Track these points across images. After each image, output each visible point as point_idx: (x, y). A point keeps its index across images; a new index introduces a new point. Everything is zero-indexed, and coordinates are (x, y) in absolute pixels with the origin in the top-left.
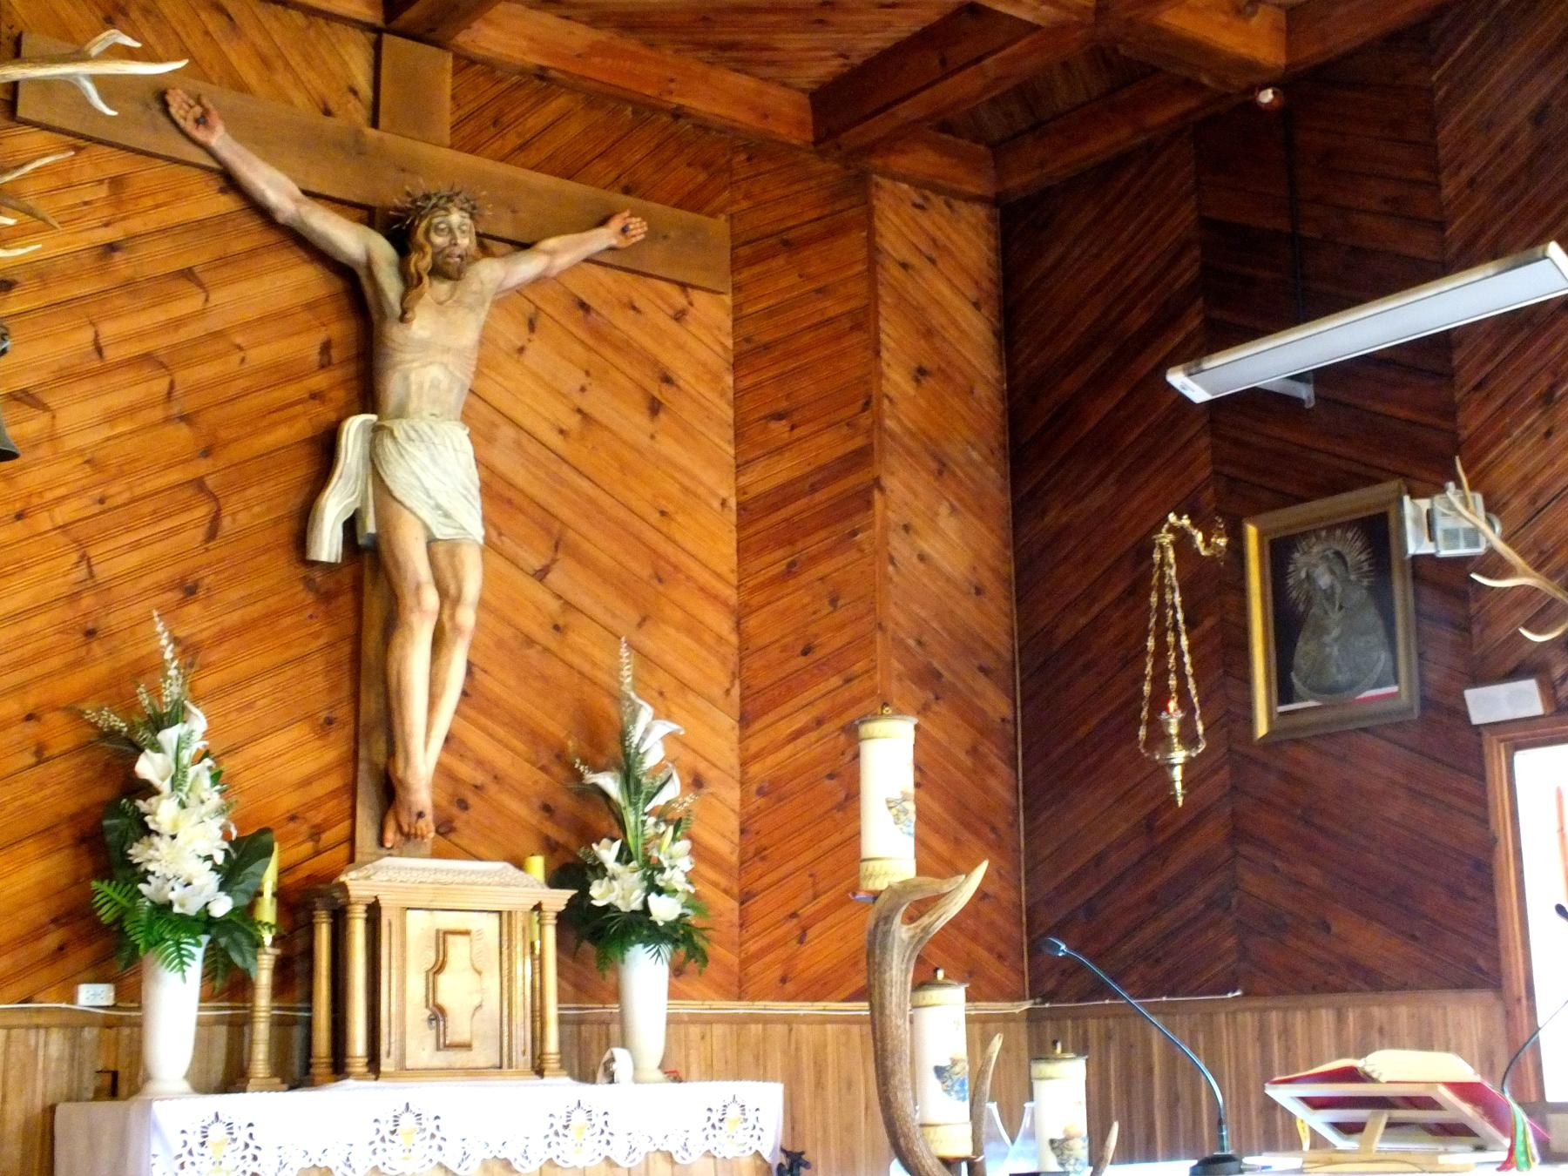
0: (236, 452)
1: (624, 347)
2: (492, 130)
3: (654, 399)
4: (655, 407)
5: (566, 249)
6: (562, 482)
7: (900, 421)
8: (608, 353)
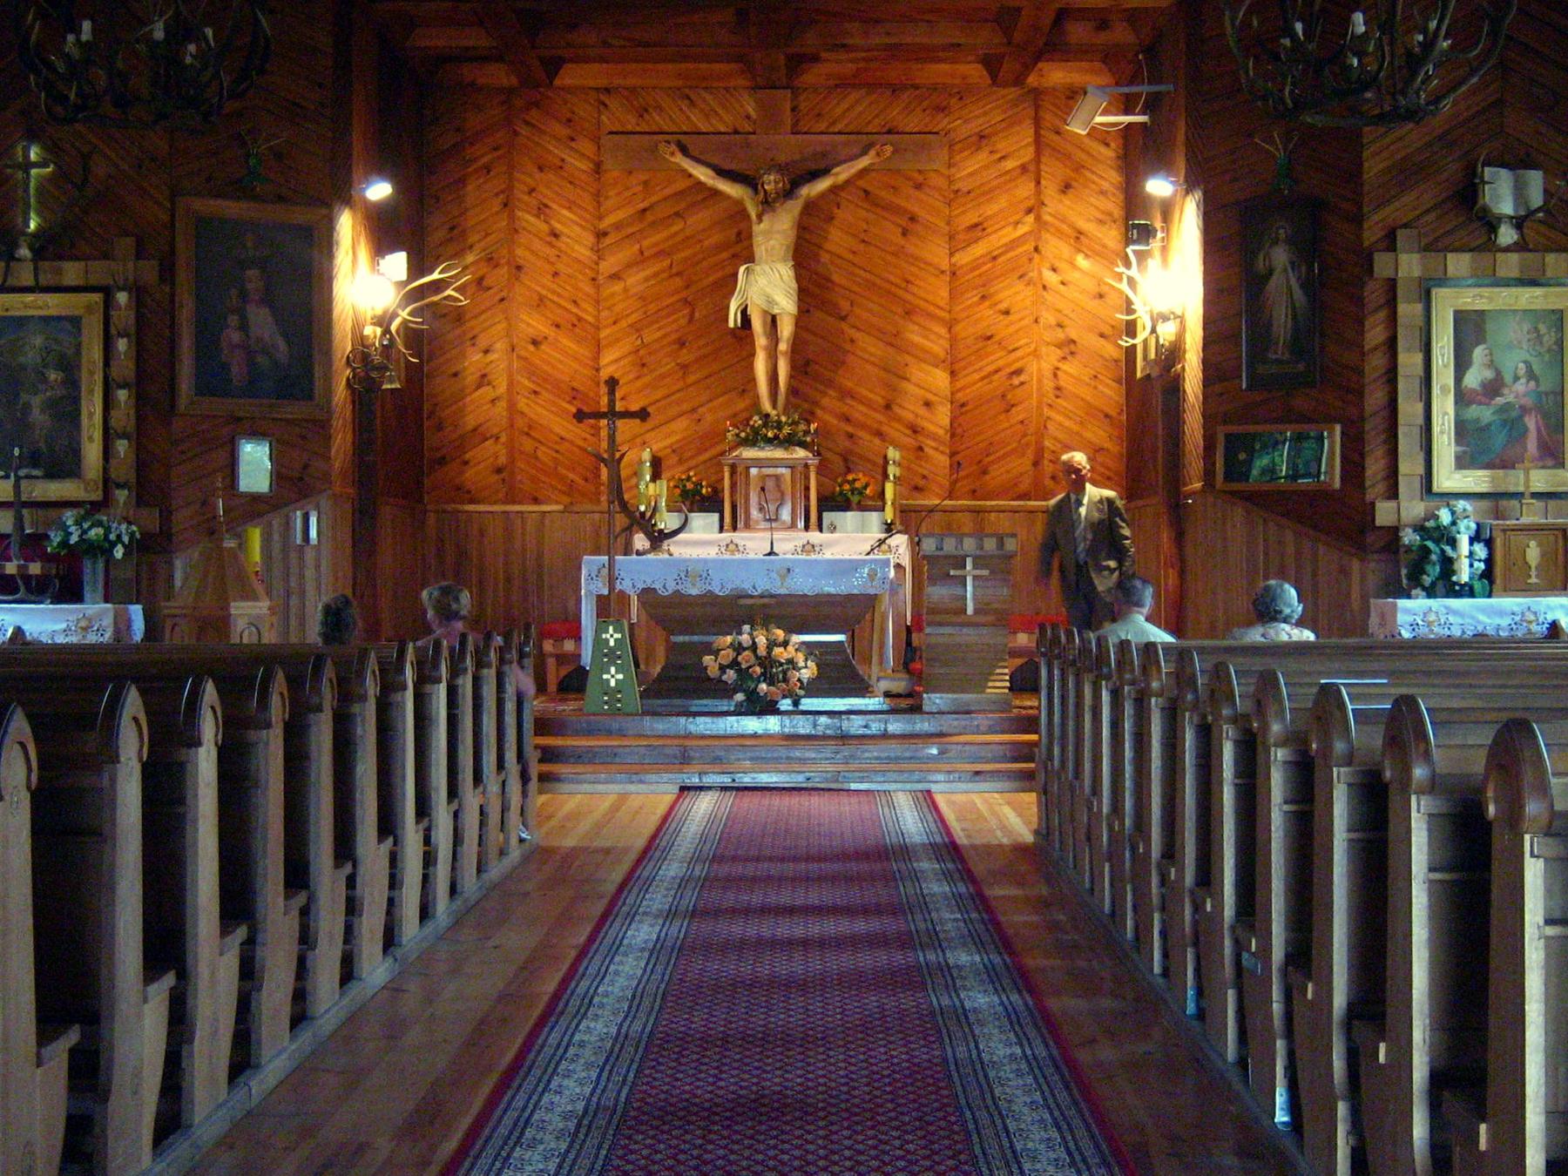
4: (905, 233)
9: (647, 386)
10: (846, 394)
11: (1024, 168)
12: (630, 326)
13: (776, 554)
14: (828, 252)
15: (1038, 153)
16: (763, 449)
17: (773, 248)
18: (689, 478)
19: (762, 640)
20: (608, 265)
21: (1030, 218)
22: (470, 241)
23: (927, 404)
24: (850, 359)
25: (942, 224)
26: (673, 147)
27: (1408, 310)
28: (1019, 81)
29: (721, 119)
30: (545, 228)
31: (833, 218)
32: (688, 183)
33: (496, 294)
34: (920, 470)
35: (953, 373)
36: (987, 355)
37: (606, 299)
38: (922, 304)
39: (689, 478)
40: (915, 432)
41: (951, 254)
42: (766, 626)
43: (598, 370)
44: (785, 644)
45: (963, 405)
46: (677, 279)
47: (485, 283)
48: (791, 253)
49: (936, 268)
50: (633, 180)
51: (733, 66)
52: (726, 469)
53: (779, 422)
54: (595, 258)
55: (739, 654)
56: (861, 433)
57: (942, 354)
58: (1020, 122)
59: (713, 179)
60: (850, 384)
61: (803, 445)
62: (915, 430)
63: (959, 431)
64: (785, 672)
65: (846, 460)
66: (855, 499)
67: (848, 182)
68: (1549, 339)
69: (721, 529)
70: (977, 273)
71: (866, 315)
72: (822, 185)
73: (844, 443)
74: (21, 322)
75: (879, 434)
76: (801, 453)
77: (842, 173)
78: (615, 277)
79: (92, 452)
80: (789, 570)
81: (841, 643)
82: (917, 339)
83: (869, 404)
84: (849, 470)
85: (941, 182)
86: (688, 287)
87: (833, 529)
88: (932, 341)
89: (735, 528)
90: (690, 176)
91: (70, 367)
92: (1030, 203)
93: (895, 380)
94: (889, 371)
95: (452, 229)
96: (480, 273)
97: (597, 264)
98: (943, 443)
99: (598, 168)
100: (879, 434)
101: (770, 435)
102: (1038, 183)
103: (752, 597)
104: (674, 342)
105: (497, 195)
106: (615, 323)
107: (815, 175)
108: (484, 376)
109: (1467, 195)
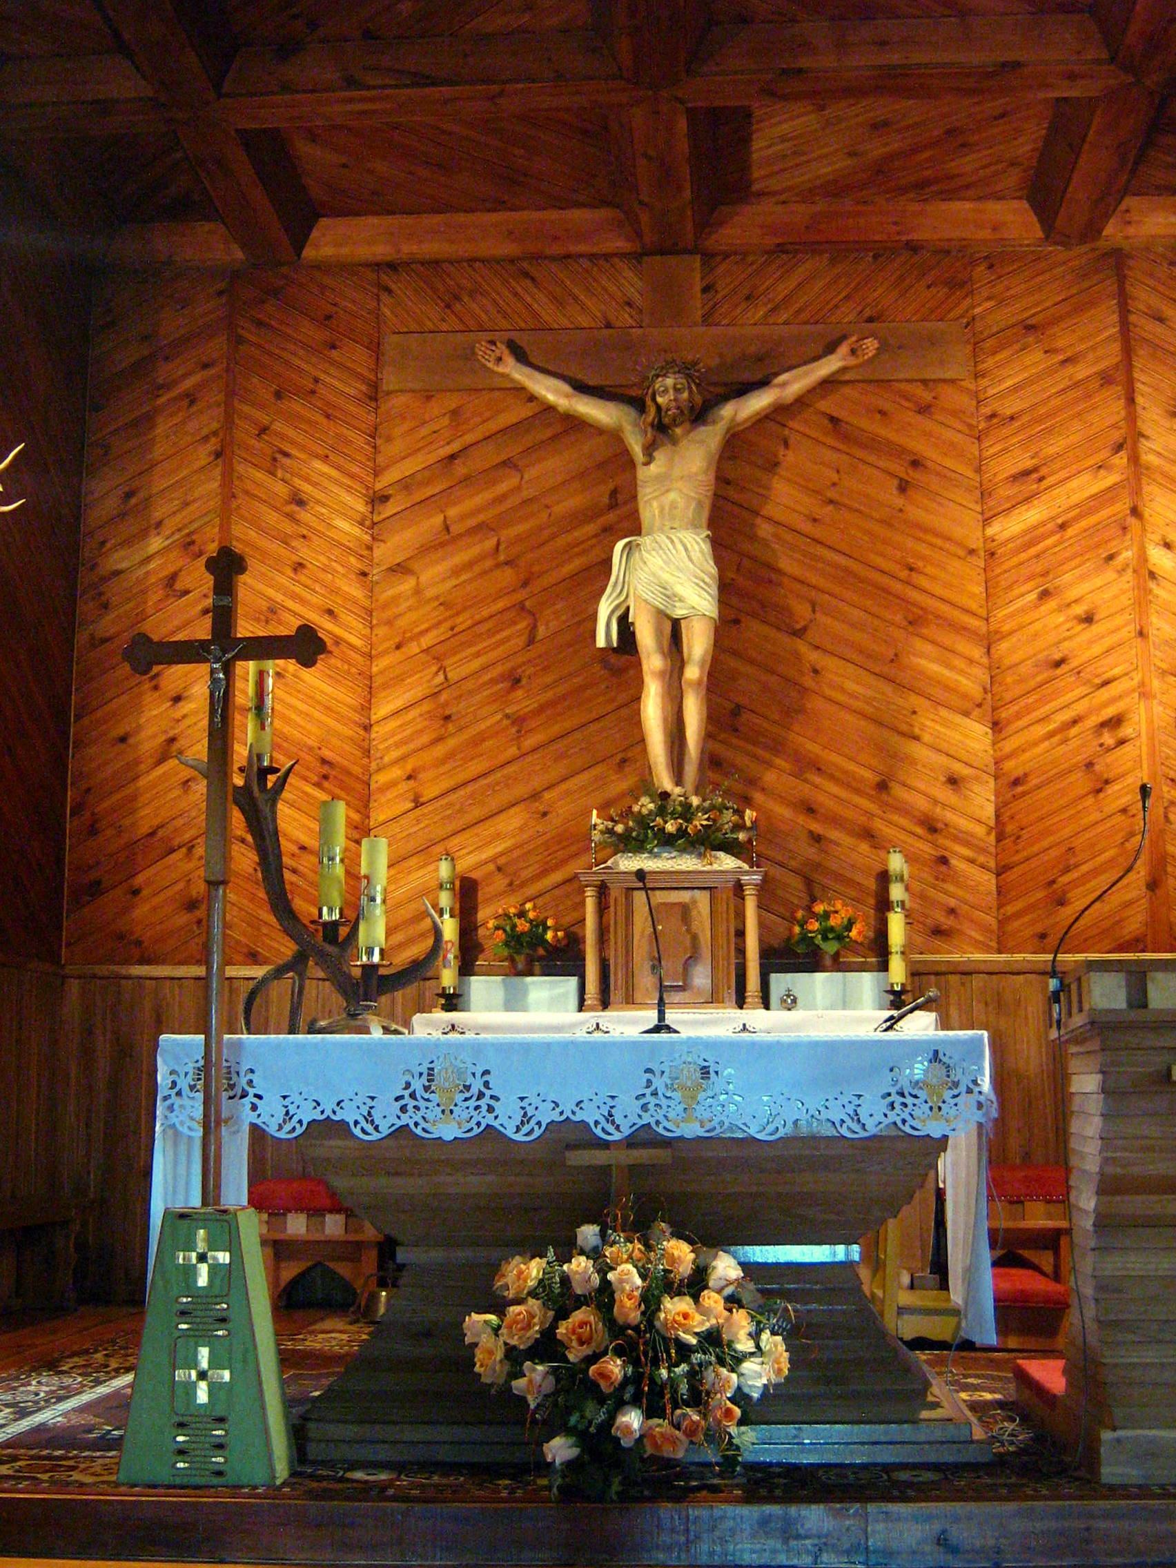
0: (546, 581)
1: (874, 444)
2: (744, 305)
3: (901, 479)
4: (903, 487)
5: (796, 379)
6: (819, 559)
7: (1159, 454)
8: (859, 453)
9: (450, 756)
10: (806, 765)
11: (1106, 379)
12: (425, 651)
13: (669, 1029)
14: (769, 519)
15: (1128, 353)
16: (657, 856)
17: (673, 506)
18: (522, 914)
19: (628, 1277)
20: (388, 552)
21: (1121, 459)
22: (157, 515)
23: (953, 781)
24: (815, 703)
25: (970, 474)
26: (502, 349)
28: (1091, 231)
29: (584, 308)
30: (282, 490)
31: (776, 464)
32: (527, 411)
33: (197, 601)
34: (942, 898)
35: (996, 726)
36: (1057, 694)
37: (385, 606)
38: (944, 608)
39: (522, 914)
40: (933, 830)
41: (986, 522)
42: (640, 1228)
43: (367, 728)
44: (696, 1284)
45: (1017, 782)
46: (509, 572)
47: (179, 586)
48: (705, 514)
49: (959, 544)
50: (435, 408)
51: (602, 213)
52: (590, 892)
53: (687, 806)
54: (367, 537)
55: (563, 1314)
56: (834, 834)
57: (976, 692)
58: (1092, 304)
59: (567, 396)
60: (813, 748)
61: (730, 847)
62: (932, 827)
63: (1010, 828)
64: (694, 1375)
65: (809, 882)
66: (831, 947)
67: (801, 402)
69: (581, 1007)
70: (1033, 551)
71: (838, 627)
72: (759, 402)
73: (809, 852)
75: (868, 835)
76: (727, 862)
77: (793, 384)
78: (400, 569)
80: (705, 1072)
81: (847, 1265)
82: (934, 668)
83: (849, 783)
84: (813, 900)
85: (966, 402)
86: (525, 584)
87: (790, 1002)
88: (962, 672)
89: (605, 1004)
90: (532, 398)
92: (1116, 436)
93: (895, 739)
94: (880, 723)
95: (129, 495)
96: (171, 569)
97: (370, 548)
98: (983, 851)
99: (374, 394)
100: (868, 835)
101: (670, 827)
102: (1131, 401)
103: (606, 1145)
104: (502, 678)
105: (206, 439)
106: (398, 647)
107: (743, 390)
108: (173, 740)
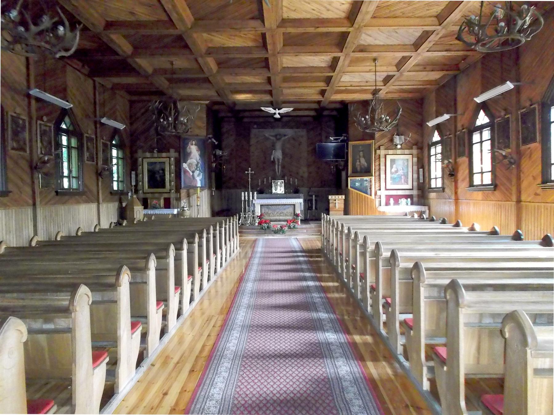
27: (382, 160)
68: (406, 164)
74: (155, 163)
79: (167, 184)
91: (163, 170)
107: (285, 136)
109: (392, 140)
